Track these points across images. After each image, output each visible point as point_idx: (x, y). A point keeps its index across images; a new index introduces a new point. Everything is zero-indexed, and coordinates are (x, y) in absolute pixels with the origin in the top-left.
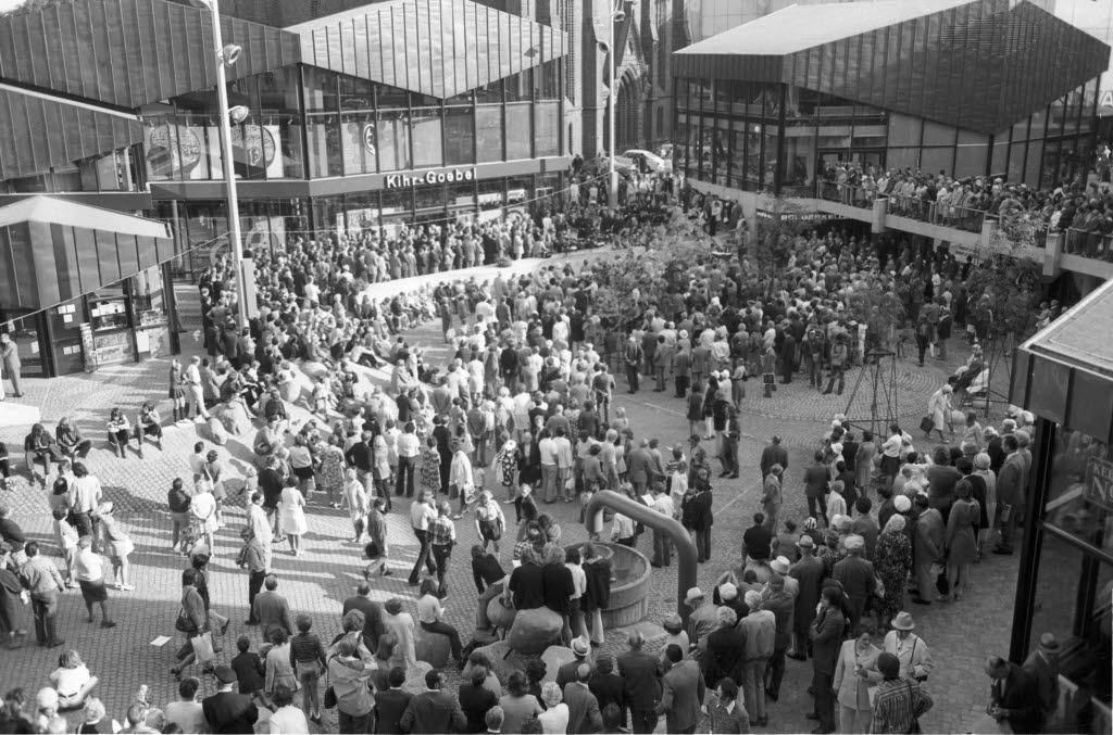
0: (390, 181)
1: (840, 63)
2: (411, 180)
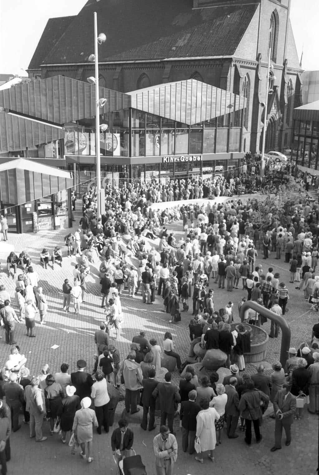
0: (165, 160)
2: (174, 159)
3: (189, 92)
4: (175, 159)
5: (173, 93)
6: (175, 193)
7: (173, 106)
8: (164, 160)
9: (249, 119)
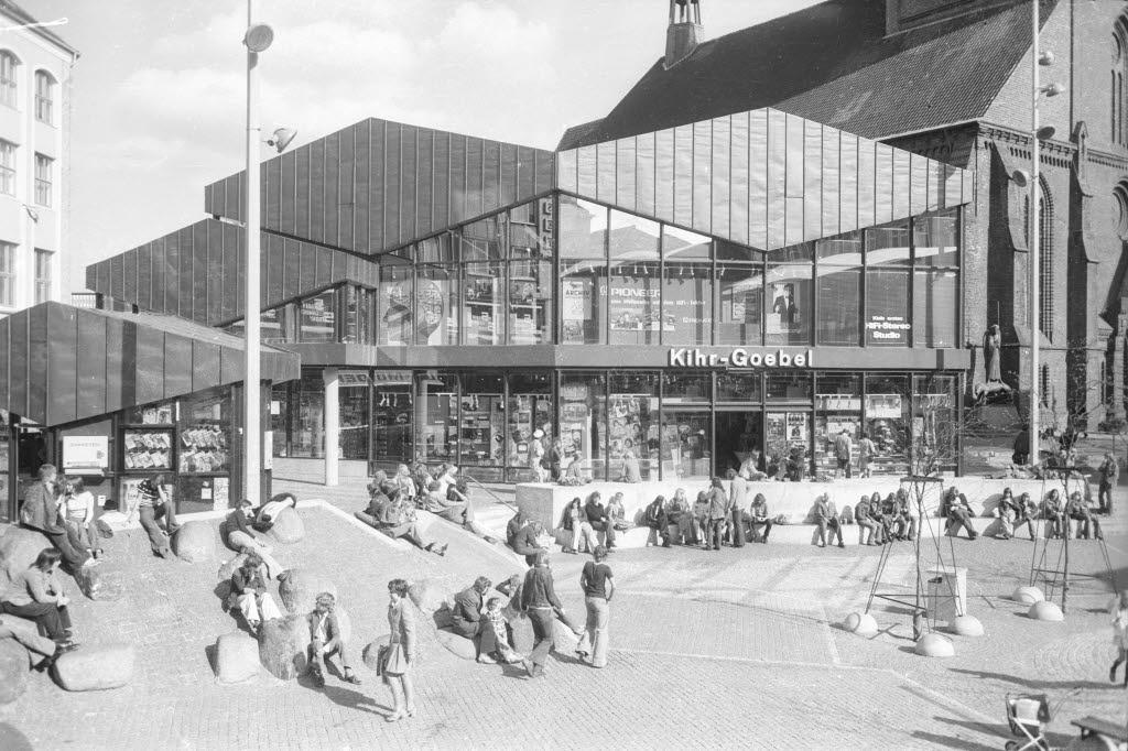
3: (759, 147)
4: (713, 357)
6: (596, 464)
7: (702, 190)
9: (1055, 309)
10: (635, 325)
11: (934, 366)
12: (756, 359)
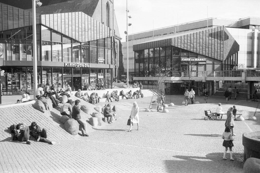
0: (66, 64)
1: (186, 41)
2: (72, 65)
5: (70, 19)
8: (66, 65)
10: (56, 57)
11: (109, 68)
12: (81, 66)
